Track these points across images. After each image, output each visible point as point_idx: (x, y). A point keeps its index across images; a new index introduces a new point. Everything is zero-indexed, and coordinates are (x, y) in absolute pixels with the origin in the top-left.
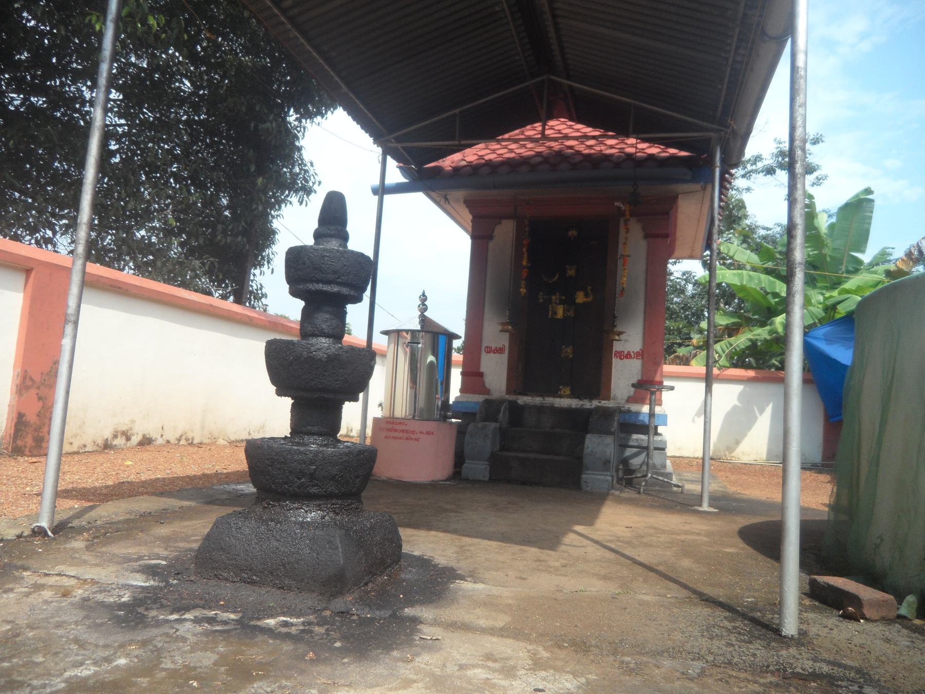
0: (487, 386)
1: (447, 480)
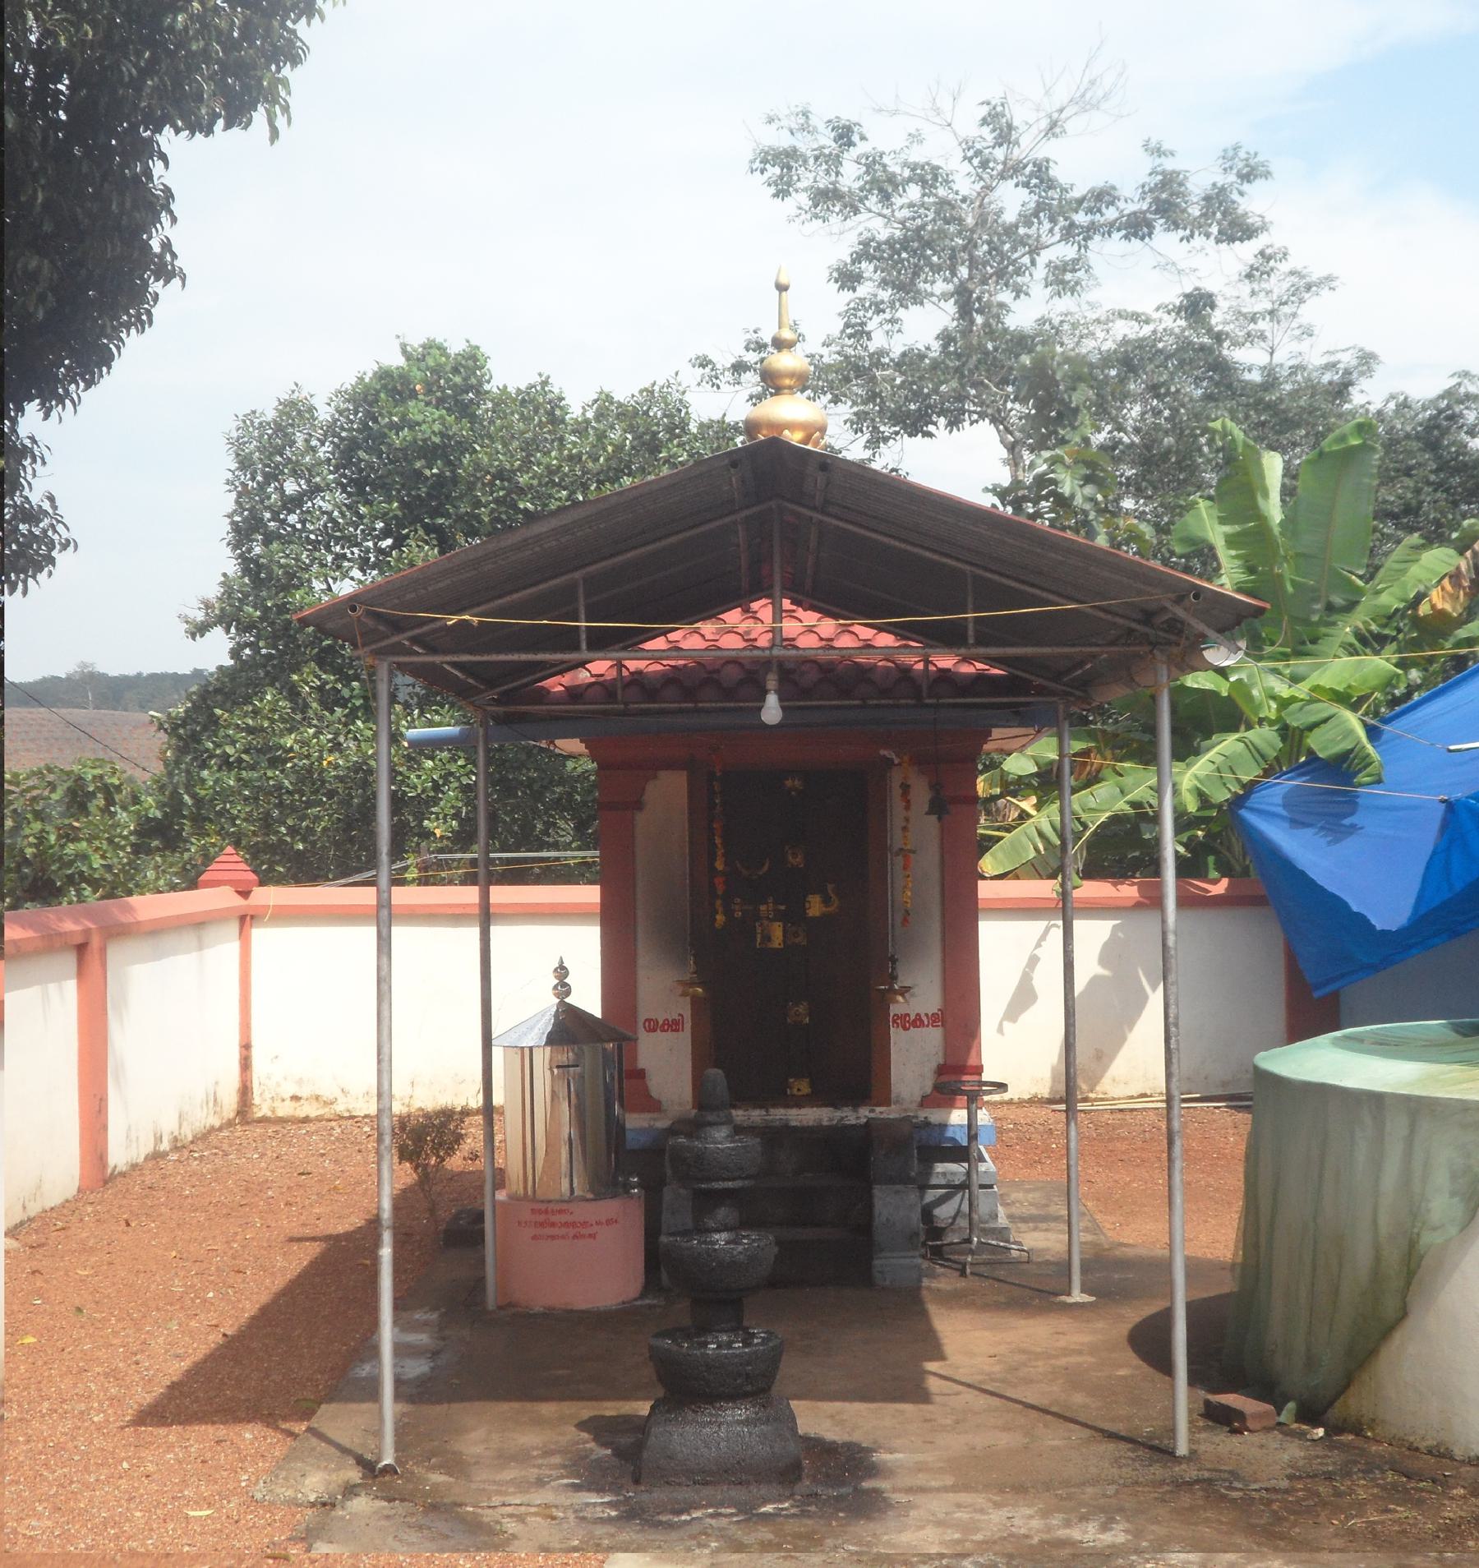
0: (654, 1094)
1: (642, 1296)
